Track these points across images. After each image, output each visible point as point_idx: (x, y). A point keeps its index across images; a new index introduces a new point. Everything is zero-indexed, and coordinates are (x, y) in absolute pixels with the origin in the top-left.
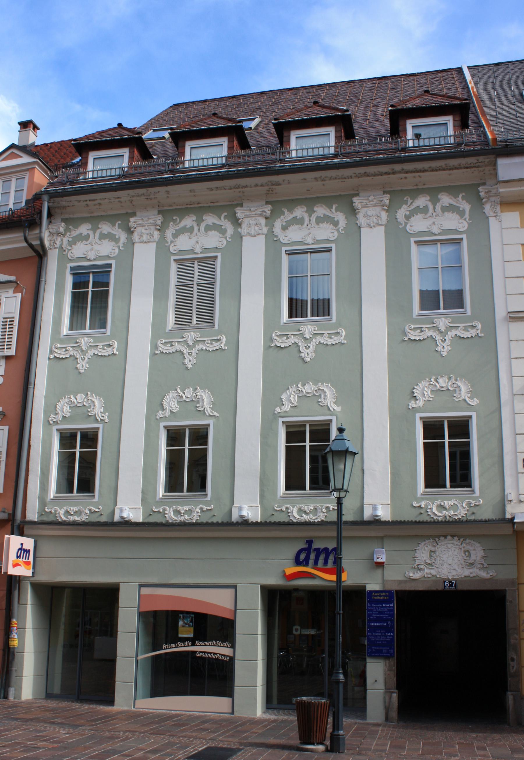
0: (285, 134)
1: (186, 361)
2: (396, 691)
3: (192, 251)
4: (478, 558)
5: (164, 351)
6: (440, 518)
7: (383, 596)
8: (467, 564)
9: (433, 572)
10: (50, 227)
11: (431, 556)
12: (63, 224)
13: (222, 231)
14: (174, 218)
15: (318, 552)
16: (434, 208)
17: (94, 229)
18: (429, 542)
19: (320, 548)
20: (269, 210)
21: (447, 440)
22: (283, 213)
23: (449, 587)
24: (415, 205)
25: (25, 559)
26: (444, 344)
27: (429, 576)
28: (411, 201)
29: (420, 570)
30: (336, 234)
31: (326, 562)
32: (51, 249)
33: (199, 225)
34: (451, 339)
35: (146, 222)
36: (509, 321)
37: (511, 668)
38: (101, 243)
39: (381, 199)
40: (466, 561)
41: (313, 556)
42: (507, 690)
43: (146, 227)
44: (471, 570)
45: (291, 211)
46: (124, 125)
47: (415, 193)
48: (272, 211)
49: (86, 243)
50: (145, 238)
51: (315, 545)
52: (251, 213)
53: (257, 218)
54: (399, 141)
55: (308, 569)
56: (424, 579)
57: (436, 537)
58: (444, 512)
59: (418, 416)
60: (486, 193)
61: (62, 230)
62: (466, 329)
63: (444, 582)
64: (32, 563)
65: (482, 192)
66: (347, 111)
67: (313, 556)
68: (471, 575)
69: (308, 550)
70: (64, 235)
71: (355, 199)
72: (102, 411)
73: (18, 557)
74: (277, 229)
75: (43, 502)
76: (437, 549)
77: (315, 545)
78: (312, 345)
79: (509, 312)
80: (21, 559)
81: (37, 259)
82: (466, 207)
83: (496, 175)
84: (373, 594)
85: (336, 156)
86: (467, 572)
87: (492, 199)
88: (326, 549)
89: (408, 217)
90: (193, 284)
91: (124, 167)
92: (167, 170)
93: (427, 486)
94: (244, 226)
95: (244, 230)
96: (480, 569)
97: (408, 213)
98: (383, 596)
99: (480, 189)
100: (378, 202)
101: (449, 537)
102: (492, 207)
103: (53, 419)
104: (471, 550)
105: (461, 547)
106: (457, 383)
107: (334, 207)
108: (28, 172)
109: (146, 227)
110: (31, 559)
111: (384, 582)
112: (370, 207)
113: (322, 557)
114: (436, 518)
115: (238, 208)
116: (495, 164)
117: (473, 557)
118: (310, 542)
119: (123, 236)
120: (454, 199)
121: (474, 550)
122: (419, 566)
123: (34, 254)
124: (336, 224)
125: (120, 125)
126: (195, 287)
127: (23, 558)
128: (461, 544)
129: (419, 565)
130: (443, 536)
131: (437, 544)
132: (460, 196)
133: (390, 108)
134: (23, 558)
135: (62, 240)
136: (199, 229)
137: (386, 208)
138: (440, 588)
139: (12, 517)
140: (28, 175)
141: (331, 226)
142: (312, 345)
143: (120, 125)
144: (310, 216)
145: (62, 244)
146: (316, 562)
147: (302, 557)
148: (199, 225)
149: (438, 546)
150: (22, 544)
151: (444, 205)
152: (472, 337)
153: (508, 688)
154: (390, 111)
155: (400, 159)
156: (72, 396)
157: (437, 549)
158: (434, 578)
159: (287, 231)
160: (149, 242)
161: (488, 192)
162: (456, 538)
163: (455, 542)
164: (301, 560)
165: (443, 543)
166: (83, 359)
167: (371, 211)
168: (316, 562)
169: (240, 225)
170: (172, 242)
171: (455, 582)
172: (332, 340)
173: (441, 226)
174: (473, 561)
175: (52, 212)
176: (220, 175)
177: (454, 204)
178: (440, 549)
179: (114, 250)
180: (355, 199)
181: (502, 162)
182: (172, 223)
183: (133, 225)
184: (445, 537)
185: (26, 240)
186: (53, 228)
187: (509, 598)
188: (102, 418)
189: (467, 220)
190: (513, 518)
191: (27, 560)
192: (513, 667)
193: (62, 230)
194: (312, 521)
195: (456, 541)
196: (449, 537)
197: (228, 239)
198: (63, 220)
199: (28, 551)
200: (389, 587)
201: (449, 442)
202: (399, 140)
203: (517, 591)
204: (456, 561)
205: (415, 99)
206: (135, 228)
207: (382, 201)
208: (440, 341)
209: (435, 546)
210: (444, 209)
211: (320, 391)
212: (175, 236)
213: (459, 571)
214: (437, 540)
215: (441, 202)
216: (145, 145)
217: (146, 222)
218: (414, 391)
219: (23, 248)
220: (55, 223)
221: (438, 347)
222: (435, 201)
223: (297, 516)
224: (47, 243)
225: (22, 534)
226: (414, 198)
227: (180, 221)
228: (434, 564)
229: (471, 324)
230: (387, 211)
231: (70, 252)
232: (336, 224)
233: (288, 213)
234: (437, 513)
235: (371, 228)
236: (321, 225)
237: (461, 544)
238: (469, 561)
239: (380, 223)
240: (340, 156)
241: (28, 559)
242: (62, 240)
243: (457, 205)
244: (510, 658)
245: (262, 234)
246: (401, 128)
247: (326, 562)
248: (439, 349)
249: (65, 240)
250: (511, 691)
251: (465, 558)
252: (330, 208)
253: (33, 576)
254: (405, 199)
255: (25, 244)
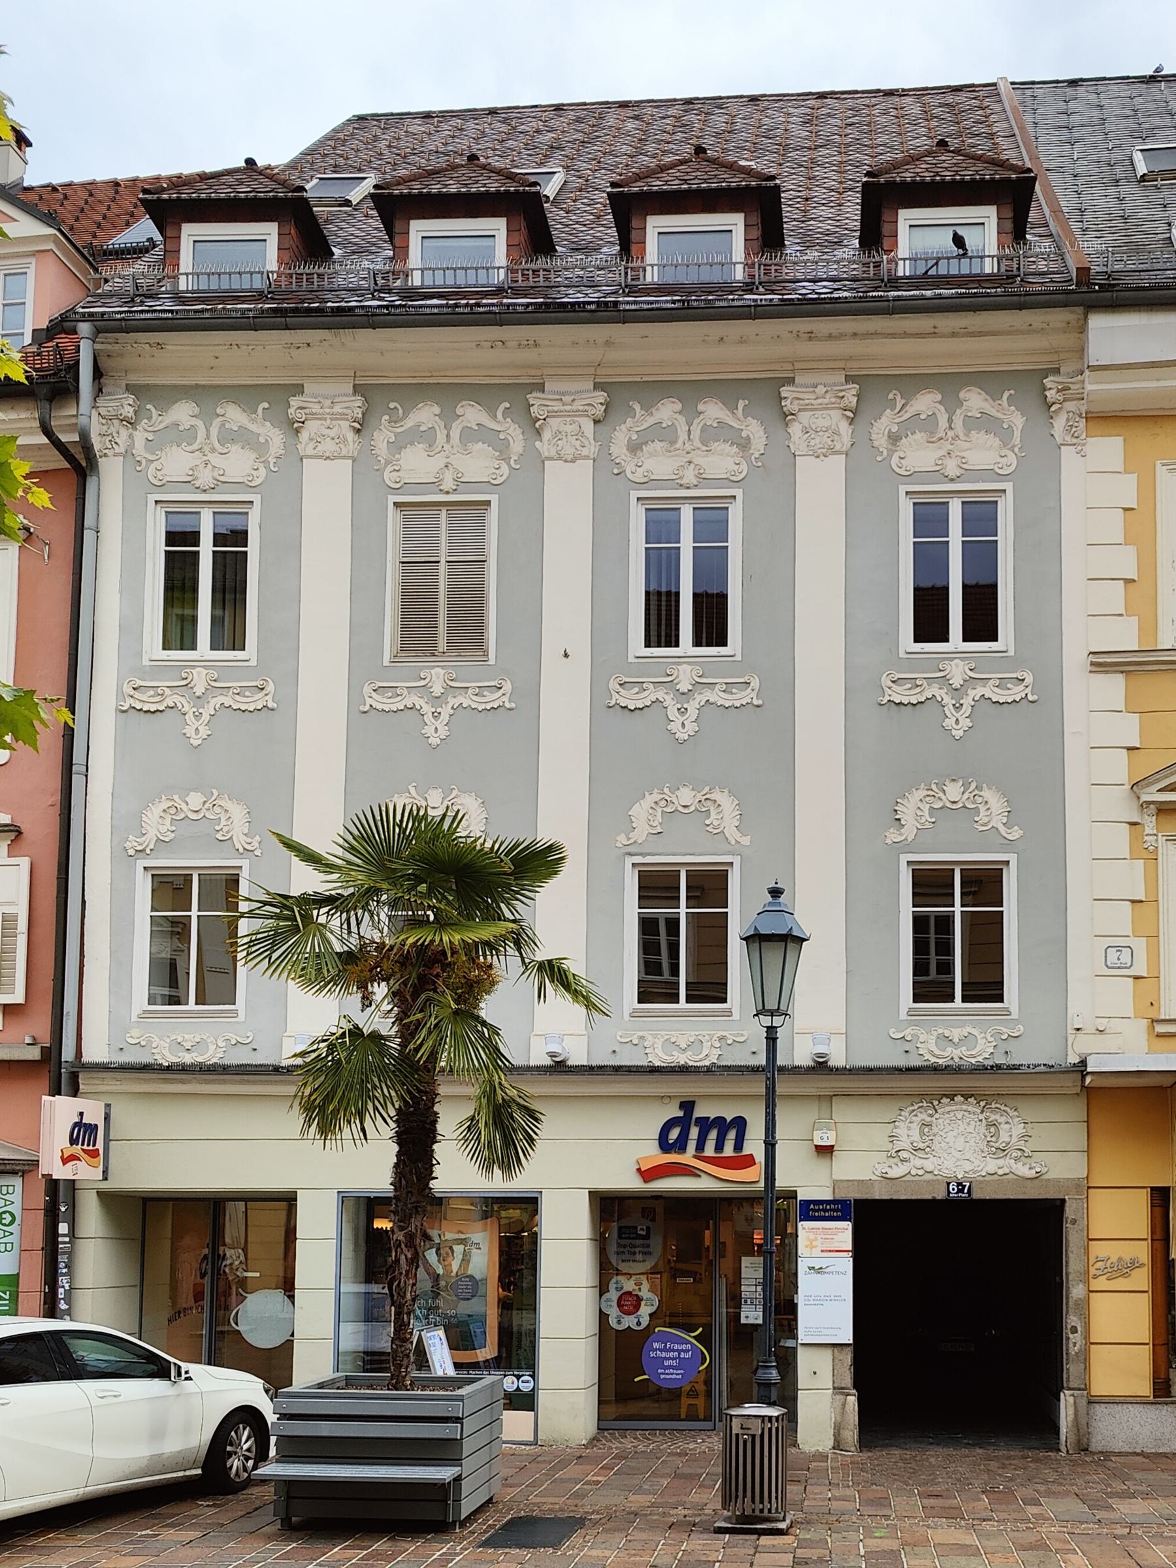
0: (635, 223)
1: (429, 730)
2: (854, 1391)
3: (436, 485)
4: (1014, 1139)
5: (380, 707)
6: (941, 1061)
7: (831, 1210)
8: (993, 1149)
9: (929, 1165)
10: (101, 402)
11: (922, 1134)
12: (131, 399)
13: (502, 449)
14: (392, 405)
15: (705, 1125)
16: (950, 420)
17: (208, 416)
18: (919, 1108)
19: (709, 1118)
20: (601, 404)
21: (958, 909)
22: (631, 412)
23: (957, 1193)
24: (910, 411)
25: (88, 1145)
26: (958, 715)
27: (920, 1172)
28: (903, 401)
29: (904, 1161)
30: (744, 467)
31: (719, 1147)
32: (105, 455)
33: (448, 427)
34: (973, 703)
35: (328, 411)
36: (1090, 672)
37: (1071, 1345)
38: (226, 450)
39: (841, 394)
40: (992, 1144)
41: (694, 1132)
42: (1063, 1388)
43: (329, 421)
44: (1001, 1162)
45: (647, 408)
46: (261, 163)
47: (913, 383)
48: (608, 406)
49: (189, 448)
50: (328, 446)
51: (699, 1112)
52: (562, 408)
53: (576, 419)
54: (885, 262)
55: (687, 1157)
56: (908, 1178)
57: (933, 1098)
58: (949, 1050)
59: (904, 859)
60: (1059, 391)
61: (128, 411)
62: (1002, 684)
63: (948, 1184)
64: (101, 1152)
65: (1050, 389)
66: (773, 178)
67: (694, 1132)
68: (1000, 1172)
69: (683, 1123)
70: (131, 423)
71: (785, 391)
72: (246, 831)
73: (73, 1141)
74: (619, 449)
75: (116, 1022)
76: (935, 1121)
77: (699, 1112)
78: (693, 707)
79: (1091, 653)
80: (80, 1146)
81: (73, 478)
82: (1017, 420)
83: (1082, 351)
84: (812, 1206)
85: (749, 287)
86: (992, 1165)
87: (1070, 406)
88: (720, 1121)
89: (894, 439)
90: (438, 562)
91: (272, 272)
92: (372, 288)
93: (917, 998)
94: (547, 435)
95: (544, 447)
96: (1016, 1160)
97: (895, 429)
98: (831, 1210)
99: (1048, 382)
100: (833, 400)
101: (959, 1099)
102: (1070, 423)
103: (136, 844)
104: (1000, 1124)
105: (981, 1117)
106: (981, 794)
107: (741, 404)
108: (33, 260)
109: (329, 421)
110: (100, 1145)
111: (836, 1183)
112: (816, 409)
113: (713, 1134)
114: (933, 1060)
115: (534, 394)
116: (1083, 329)
117: (1004, 1137)
118: (688, 1106)
119: (275, 437)
120: (991, 402)
121: (1007, 1123)
122: (900, 1154)
123: (67, 465)
124: (744, 445)
125: (250, 162)
126: (443, 568)
127: (83, 1144)
128: (982, 1112)
129: (899, 1151)
130: (947, 1096)
131: (936, 1112)
132: (1006, 395)
133: (865, 179)
134: (83, 1144)
135: (131, 436)
136: (448, 436)
137: (850, 414)
138: (940, 1195)
139: (51, 1054)
140: (33, 266)
141: (735, 449)
142: (693, 707)
143: (250, 162)
144: (690, 424)
145: (132, 446)
146: (700, 1146)
147: (674, 1134)
148: (448, 427)
149: (937, 1116)
150: (81, 1114)
151: (970, 414)
152: (1015, 701)
153: (1065, 1385)
154: (865, 185)
155: (886, 303)
156: (176, 797)
157: (935, 1121)
158: (928, 1177)
159: (639, 453)
160: (336, 458)
161: (1064, 389)
162: (972, 1100)
163: (970, 1108)
164: (671, 1142)
165: (948, 1108)
166: (198, 716)
167: (821, 420)
168: (700, 1146)
169: (538, 432)
170: (388, 462)
171: (968, 1184)
172: (735, 697)
173: (964, 461)
174: (1004, 1145)
175: (104, 363)
176: (495, 313)
177: (993, 412)
178: (940, 1121)
179: (257, 469)
180: (785, 391)
181: (1098, 322)
182: (386, 417)
183: (300, 416)
184: (952, 1097)
185: (47, 431)
186: (107, 405)
187: (1069, 1212)
188: (248, 847)
189: (1016, 450)
190: (1083, 1063)
191: (91, 1148)
192: (1075, 1344)
193: (128, 411)
194: (691, 1064)
195: (972, 1106)
196: (959, 1099)
197: (512, 462)
198: (130, 388)
199: (93, 1128)
200: (841, 1195)
201: (953, 906)
202: (885, 257)
203: (1085, 1201)
204: (972, 1142)
205: (917, 160)
206: (303, 423)
207: (843, 397)
208: (951, 707)
209: (931, 1116)
210: (971, 424)
211: (709, 803)
212: (397, 446)
213: (977, 1163)
214: (935, 1103)
215: (964, 408)
216: (313, 217)
217: (328, 411)
218: (896, 808)
219: (39, 447)
220: (109, 394)
221: (947, 720)
222: (952, 403)
223: (661, 1054)
224: (97, 444)
225: (75, 1092)
226: (908, 397)
227: (406, 415)
228: (928, 1149)
229: (1014, 675)
230: (852, 421)
231: (153, 466)
232: (744, 445)
233: (643, 412)
234: (937, 1052)
235: (818, 457)
236: (714, 446)
237: (982, 1112)
238: (997, 1145)
239: (838, 447)
240: (757, 288)
241: (94, 1145)
242: (131, 436)
243: (1000, 415)
244: (1069, 1327)
245: (587, 458)
246: (886, 229)
247: (719, 1147)
248: (949, 723)
249: (140, 436)
250: (1070, 1389)
251: (989, 1139)
252: (733, 408)
253: (105, 1179)
254: (891, 396)
255: (44, 440)
